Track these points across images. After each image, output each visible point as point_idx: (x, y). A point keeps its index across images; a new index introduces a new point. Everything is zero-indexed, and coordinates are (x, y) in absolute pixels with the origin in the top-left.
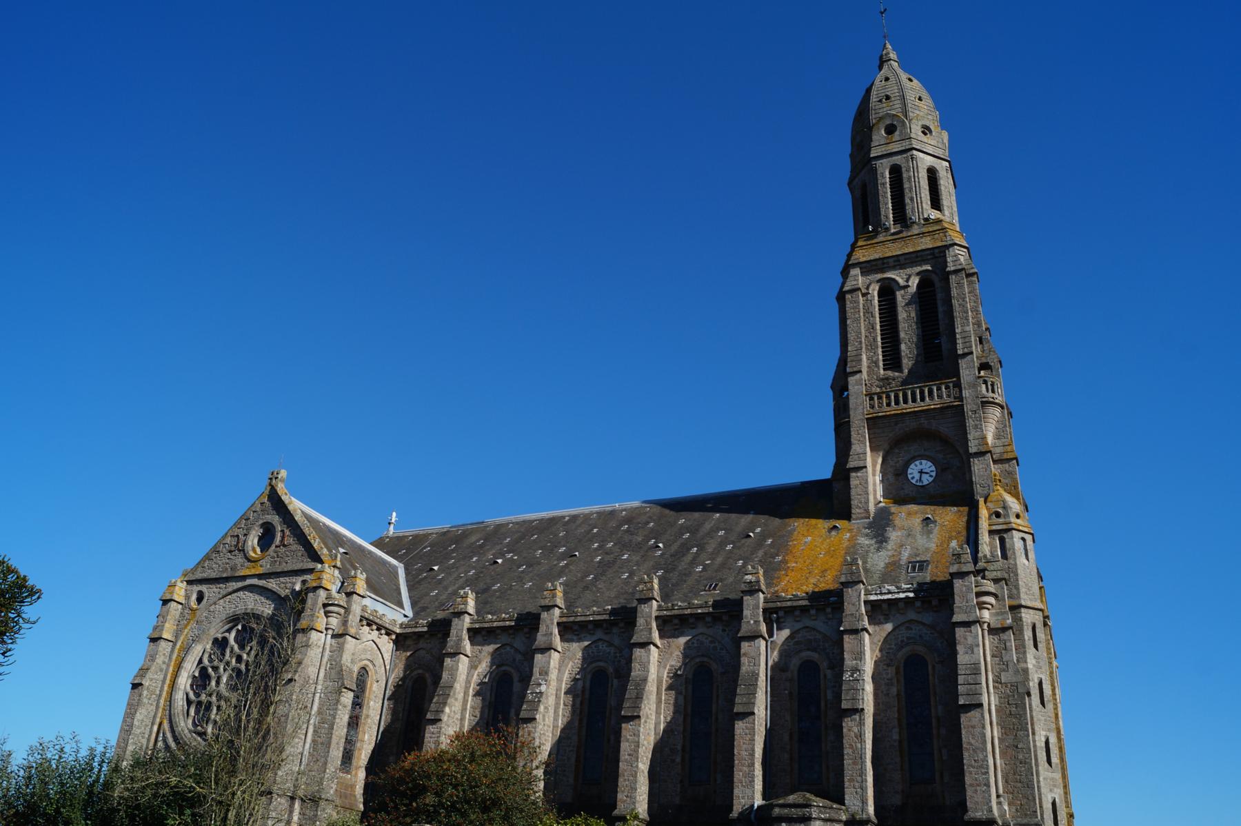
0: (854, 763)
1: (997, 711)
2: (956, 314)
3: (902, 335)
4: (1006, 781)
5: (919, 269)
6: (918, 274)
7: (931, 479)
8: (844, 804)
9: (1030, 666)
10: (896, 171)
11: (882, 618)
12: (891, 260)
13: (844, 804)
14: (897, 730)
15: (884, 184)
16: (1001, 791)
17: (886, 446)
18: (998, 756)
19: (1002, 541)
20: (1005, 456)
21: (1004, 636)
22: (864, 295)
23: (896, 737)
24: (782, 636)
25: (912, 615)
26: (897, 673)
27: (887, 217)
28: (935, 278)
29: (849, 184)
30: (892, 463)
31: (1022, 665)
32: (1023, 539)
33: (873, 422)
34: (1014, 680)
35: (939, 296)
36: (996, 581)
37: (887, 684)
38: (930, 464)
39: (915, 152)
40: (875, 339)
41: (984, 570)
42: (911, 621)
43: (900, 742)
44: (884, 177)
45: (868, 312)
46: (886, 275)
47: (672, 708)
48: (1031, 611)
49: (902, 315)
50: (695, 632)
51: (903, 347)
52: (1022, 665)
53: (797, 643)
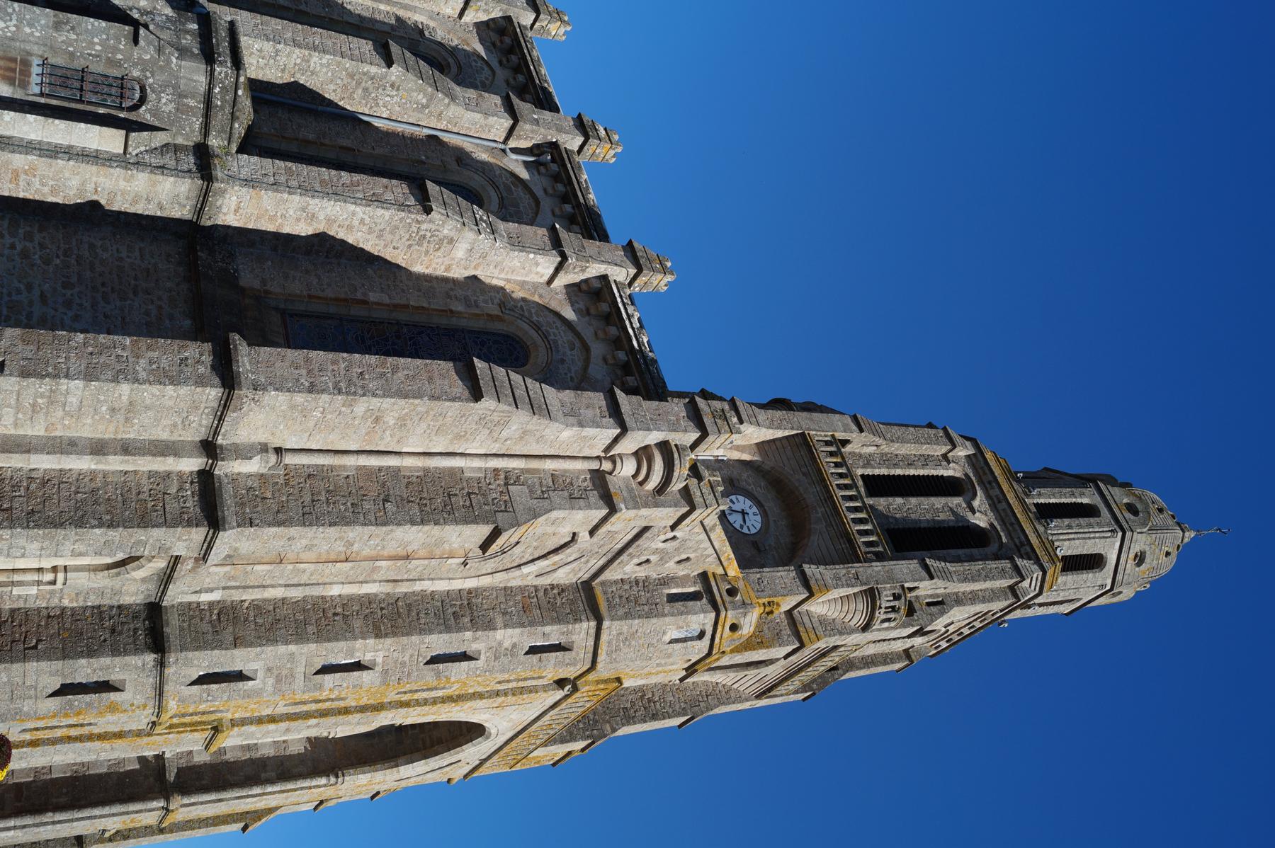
0: (322, 182)
1: (452, 472)
2: (967, 566)
3: (914, 500)
4: (312, 474)
5: (996, 524)
6: (992, 525)
7: (737, 526)
8: (241, 150)
9: (500, 634)
10: (1087, 511)
11: (581, 306)
12: (997, 492)
13: (241, 150)
14: (387, 301)
15: (1073, 495)
16: (290, 459)
17: (768, 465)
18: (364, 461)
19: (694, 596)
20: (801, 629)
21: (594, 496)
22: (945, 456)
23: (373, 297)
24: (516, 165)
25: (598, 349)
26: (491, 317)
27: (1040, 495)
28: (993, 547)
29: (1045, 469)
30: (745, 475)
31: (499, 620)
32: (701, 635)
33: (802, 442)
34: (518, 507)
35: (975, 551)
36: (686, 492)
37: (466, 299)
38: (758, 526)
39: (1120, 534)
40: (896, 466)
41: (700, 478)
42: (586, 348)
43: (365, 302)
44: (1082, 494)
45: (926, 460)
46: (978, 488)
47: (367, 14)
48: (591, 642)
49: (939, 502)
50: (495, 64)
51: (899, 500)
52: (499, 620)
53: (509, 190)
